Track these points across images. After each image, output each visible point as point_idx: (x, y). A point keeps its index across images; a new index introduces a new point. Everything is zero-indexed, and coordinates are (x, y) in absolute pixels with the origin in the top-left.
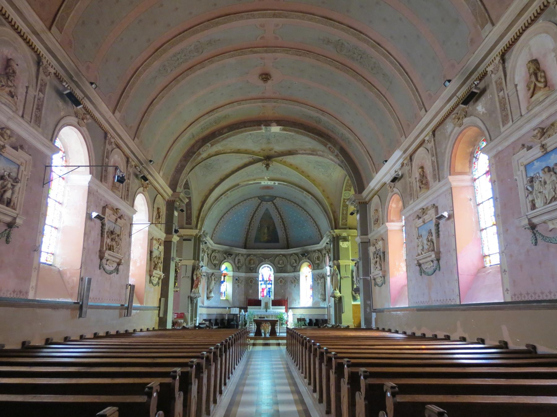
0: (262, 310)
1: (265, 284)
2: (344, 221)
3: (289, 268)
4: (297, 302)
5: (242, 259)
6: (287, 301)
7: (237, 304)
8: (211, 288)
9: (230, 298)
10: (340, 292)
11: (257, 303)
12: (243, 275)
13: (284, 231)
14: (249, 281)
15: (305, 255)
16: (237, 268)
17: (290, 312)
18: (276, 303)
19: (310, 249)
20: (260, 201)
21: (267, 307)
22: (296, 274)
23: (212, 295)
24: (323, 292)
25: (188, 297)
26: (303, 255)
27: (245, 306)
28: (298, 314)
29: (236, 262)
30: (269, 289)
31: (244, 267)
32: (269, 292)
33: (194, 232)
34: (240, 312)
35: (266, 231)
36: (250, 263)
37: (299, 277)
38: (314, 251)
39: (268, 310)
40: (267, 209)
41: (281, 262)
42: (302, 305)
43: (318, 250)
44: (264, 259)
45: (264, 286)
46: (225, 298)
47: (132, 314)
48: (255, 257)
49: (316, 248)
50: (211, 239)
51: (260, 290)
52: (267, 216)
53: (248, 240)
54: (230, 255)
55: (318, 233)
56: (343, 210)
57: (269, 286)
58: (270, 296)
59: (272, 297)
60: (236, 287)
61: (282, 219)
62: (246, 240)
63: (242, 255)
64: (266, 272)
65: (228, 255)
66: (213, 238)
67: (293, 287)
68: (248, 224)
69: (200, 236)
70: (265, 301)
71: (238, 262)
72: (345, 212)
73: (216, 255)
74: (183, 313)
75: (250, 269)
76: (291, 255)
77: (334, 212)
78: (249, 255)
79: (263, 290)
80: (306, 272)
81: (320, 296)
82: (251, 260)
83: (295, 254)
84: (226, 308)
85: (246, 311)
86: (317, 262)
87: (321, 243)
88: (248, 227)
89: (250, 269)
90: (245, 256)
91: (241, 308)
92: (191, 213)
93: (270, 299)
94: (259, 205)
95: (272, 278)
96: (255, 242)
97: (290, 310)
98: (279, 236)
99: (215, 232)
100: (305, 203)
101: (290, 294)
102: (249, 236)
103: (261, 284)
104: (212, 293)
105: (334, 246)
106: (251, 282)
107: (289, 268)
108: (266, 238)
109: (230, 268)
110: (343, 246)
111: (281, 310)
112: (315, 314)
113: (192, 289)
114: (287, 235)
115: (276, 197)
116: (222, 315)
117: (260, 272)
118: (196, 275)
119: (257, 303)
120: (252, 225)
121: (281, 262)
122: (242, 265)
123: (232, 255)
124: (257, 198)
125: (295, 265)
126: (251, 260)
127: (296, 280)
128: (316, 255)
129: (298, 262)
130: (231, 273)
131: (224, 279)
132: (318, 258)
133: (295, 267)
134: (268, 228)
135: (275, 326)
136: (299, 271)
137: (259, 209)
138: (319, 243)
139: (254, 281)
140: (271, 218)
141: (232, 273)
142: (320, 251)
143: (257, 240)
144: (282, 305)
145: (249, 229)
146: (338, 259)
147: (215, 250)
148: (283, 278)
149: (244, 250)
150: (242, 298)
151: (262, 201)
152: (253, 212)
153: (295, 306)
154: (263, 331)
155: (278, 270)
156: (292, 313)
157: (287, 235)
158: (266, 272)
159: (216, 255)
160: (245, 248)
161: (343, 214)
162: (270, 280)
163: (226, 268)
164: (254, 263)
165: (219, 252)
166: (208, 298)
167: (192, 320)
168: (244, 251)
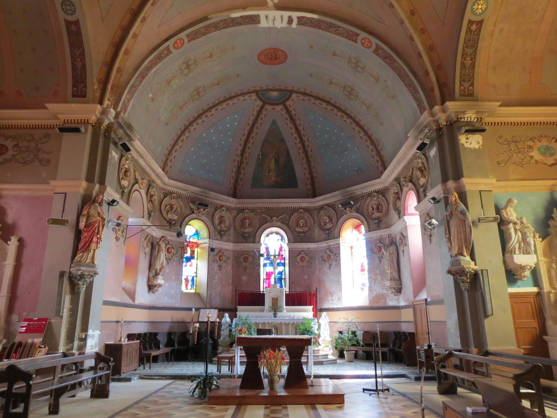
0: (265, 313)
1: (272, 264)
2: (466, 85)
3: (317, 231)
4: (335, 297)
5: (228, 217)
6: (315, 295)
7: (217, 302)
8: (158, 267)
9: (203, 291)
10: (473, 258)
11: (257, 299)
12: (229, 246)
13: (305, 166)
14: (242, 258)
15: (353, 206)
16: (217, 231)
17: (325, 318)
18: (295, 299)
19: (359, 192)
20: (260, 103)
21: (275, 308)
22: (331, 243)
23: (160, 280)
24: (395, 275)
25: (62, 275)
26: (346, 204)
27: (233, 307)
28: (342, 320)
29: (217, 221)
30: (280, 273)
31: (232, 231)
32: (280, 279)
33: (90, 112)
34: (221, 317)
35: (272, 165)
36: (243, 225)
37: (339, 248)
38: (370, 195)
39: (279, 314)
40: (274, 122)
41: (301, 222)
42: (346, 303)
43: (377, 192)
44: (267, 218)
45: (269, 269)
46: (193, 291)
47: (269, 328)
48: (252, 214)
49: (372, 189)
50: (163, 170)
51: (263, 276)
52: (274, 138)
53: (240, 182)
54: (203, 205)
55: (377, 158)
56: (464, 56)
57: (281, 269)
58: (281, 286)
59: (286, 289)
60: (216, 268)
61: (302, 142)
62: (236, 181)
63: (229, 209)
64: (274, 241)
65: (198, 206)
66: (167, 168)
67: (326, 269)
68: (239, 152)
69: (110, 127)
70: (273, 295)
71: (221, 223)
72: (468, 62)
73: (173, 202)
74: (46, 320)
75: (243, 236)
76: (322, 208)
77: (438, 68)
78: (242, 210)
79: (269, 275)
80: (353, 241)
81: (388, 283)
82: (245, 219)
83: (327, 205)
84: (190, 309)
85: (233, 315)
86: (376, 215)
87: (383, 177)
88: (238, 159)
89: (243, 236)
90: (235, 212)
91: (222, 311)
92: (84, 67)
93: (281, 292)
94: (260, 112)
95: (286, 254)
96: (253, 186)
97: (324, 314)
98: (297, 176)
99: (171, 157)
100: (350, 92)
101: (321, 282)
102: (242, 176)
103: (265, 265)
104: (160, 277)
105: (441, 151)
106: (246, 260)
107: (317, 231)
108: (273, 177)
109: (204, 233)
110: (467, 145)
111: (307, 312)
112: (377, 321)
113: (74, 255)
114: (311, 173)
115: (292, 92)
116: (183, 323)
117: (262, 242)
118: (88, 216)
119: (257, 299)
120: (246, 155)
121: (301, 222)
122: (229, 229)
123: (207, 206)
124: (254, 96)
125: (329, 226)
126: (245, 219)
127: (333, 255)
128: (373, 202)
129: (334, 220)
130: (204, 241)
131: (193, 252)
132: (378, 208)
133: (329, 229)
134: (277, 161)
135: (300, 355)
136: (339, 236)
137: (260, 121)
138: (380, 177)
139: (250, 259)
140: (283, 140)
141: (207, 241)
142: (382, 192)
143: (257, 181)
144: (306, 304)
145: (241, 162)
146: (458, 175)
147: (172, 193)
148: (307, 252)
149: (231, 199)
150: (228, 291)
151: (265, 103)
152: (248, 128)
153: (331, 306)
154: (264, 370)
155: (295, 237)
156: (328, 320)
157: (311, 173)
158: (274, 241)
159: (173, 202)
160: (235, 196)
161: (463, 66)
162: (280, 256)
163: (197, 233)
164: (250, 225)
165: (179, 196)
166: (151, 287)
167: (70, 338)
168: (232, 202)
